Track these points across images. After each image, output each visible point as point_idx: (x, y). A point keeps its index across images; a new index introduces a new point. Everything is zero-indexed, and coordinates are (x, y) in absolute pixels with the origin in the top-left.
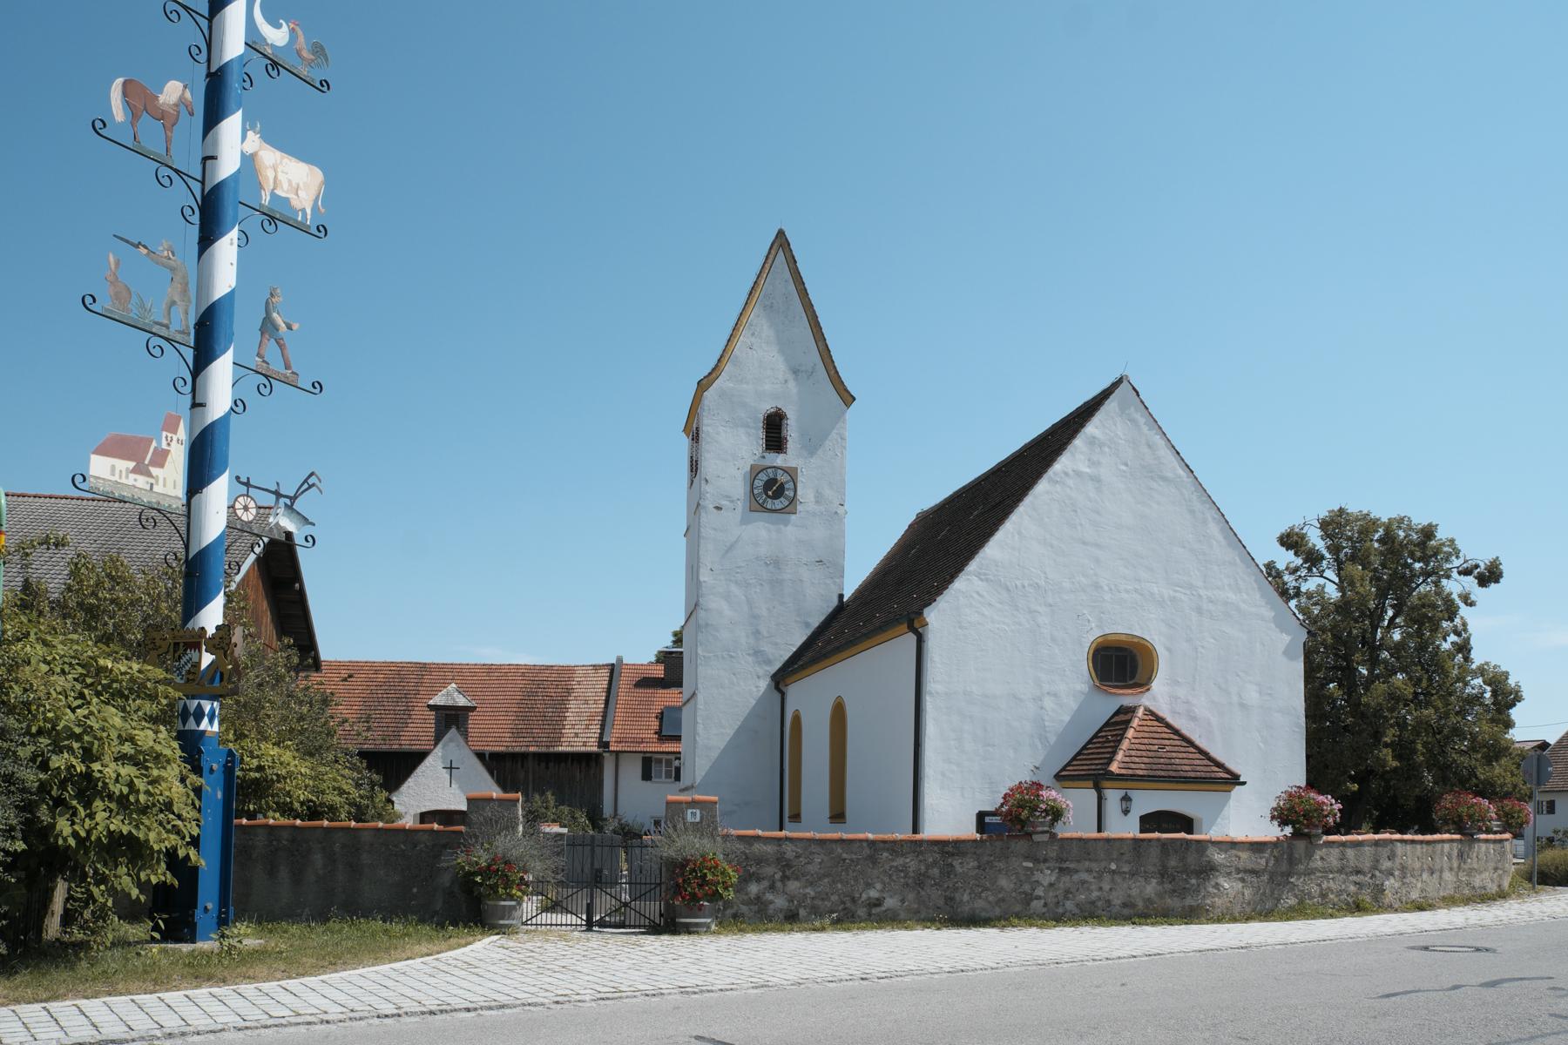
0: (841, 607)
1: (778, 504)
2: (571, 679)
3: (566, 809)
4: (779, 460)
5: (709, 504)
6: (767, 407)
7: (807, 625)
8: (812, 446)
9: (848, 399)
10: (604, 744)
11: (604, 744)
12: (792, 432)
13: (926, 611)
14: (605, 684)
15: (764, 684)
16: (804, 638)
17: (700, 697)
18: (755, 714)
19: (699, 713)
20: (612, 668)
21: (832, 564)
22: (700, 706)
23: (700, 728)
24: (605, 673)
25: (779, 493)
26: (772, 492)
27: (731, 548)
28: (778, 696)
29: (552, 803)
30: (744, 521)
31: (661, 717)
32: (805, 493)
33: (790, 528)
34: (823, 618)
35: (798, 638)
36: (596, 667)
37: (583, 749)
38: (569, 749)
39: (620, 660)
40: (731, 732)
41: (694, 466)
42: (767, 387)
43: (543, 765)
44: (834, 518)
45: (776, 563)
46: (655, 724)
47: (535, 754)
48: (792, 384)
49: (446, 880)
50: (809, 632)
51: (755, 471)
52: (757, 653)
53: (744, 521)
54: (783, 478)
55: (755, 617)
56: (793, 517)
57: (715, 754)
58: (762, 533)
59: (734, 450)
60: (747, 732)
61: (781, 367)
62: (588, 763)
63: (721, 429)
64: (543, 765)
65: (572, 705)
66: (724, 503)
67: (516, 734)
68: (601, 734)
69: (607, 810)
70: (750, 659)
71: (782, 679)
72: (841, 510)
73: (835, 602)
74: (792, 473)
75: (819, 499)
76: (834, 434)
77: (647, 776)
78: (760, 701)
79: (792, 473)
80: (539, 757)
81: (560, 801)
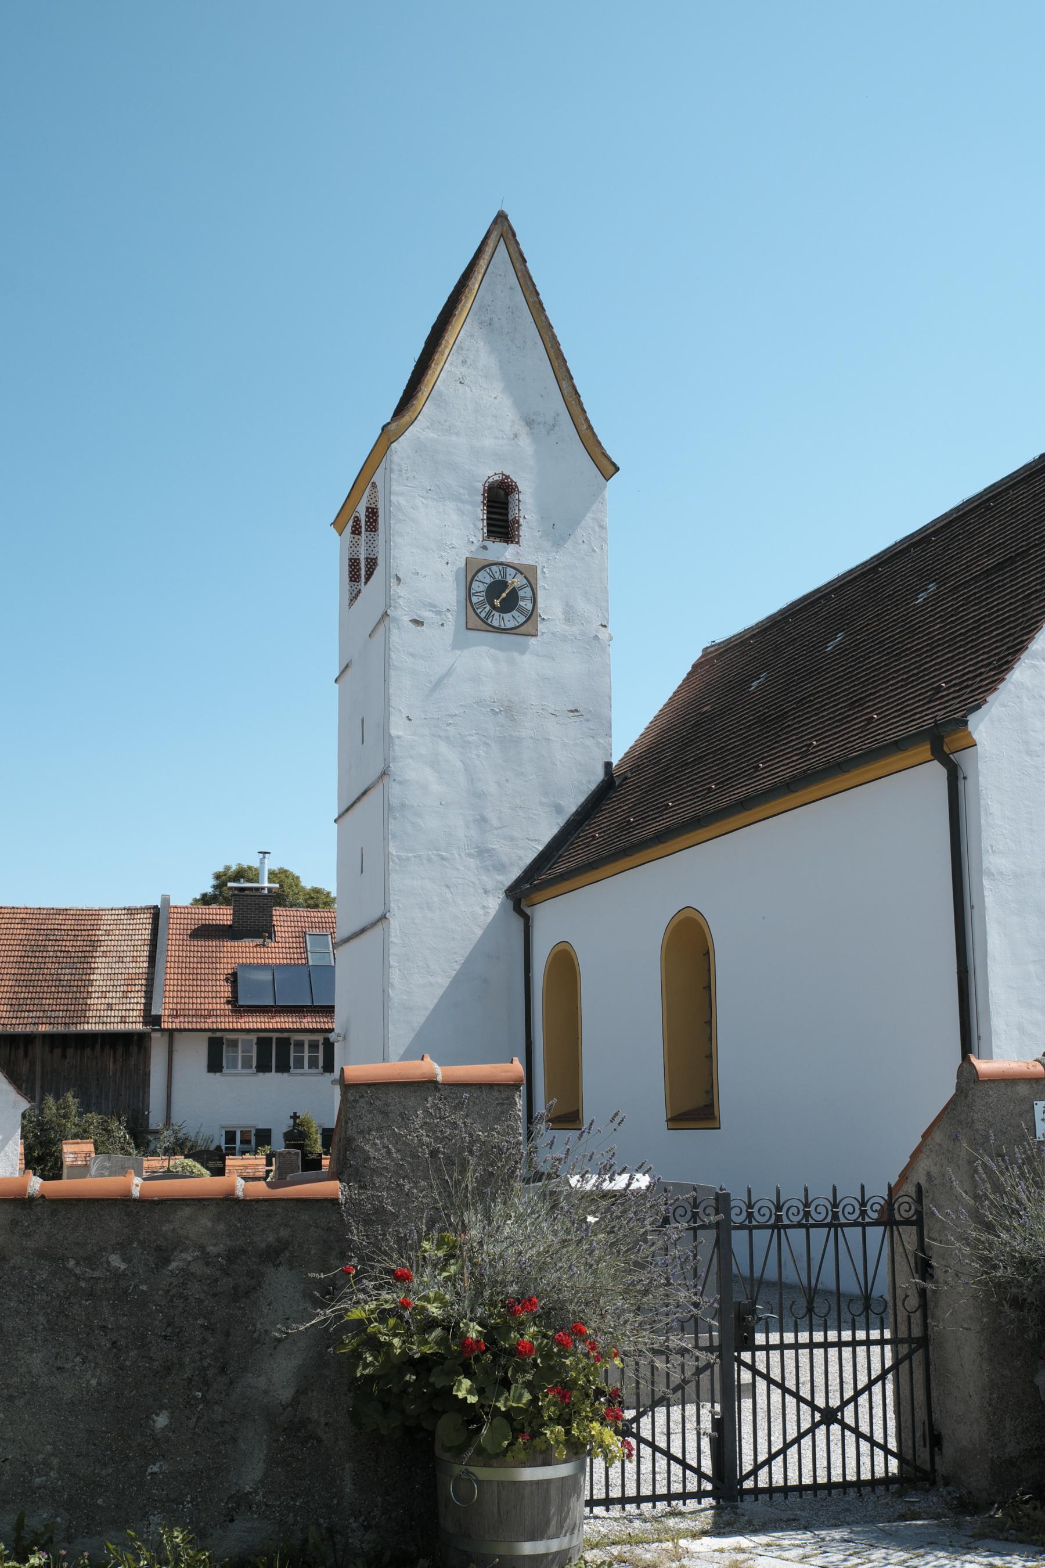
0: (610, 786)
1: (509, 620)
2: (95, 927)
3: (94, 1117)
4: (508, 553)
5: (402, 614)
6: (488, 472)
7: (559, 809)
8: (559, 533)
9: (608, 468)
10: (152, 1020)
11: (152, 1020)
12: (527, 510)
13: (972, 719)
14: (147, 934)
15: (495, 902)
16: (555, 830)
17: (395, 923)
18: (483, 952)
19: (393, 950)
20: (156, 913)
21: (590, 714)
22: (395, 937)
23: (395, 976)
24: (146, 919)
25: (510, 604)
26: (500, 602)
27: (438, 684)
28: (518, 923)
29: (74, 1109)
30: (458, 644)
31: (233, 979)
32: (550, 605)
33: (527, 658)
34: (581, 799)
35: (545, 831)
36: (131, 911)
37: (121, 1027)
38: (100, 1028)
39: (166, 900)
40: (444, 982)
41: (360, 571)
42: (488, 443)
43: (58, 1052)
44: (594, 645)
45: (508, 711)
46: (226, 990)
47: (45, 1036)
48: (525, 443)
49: (278, 1377)
50: (562, 821)
51: (472, 570)
52: (482, 852)
53: (458, 644)
54: (515, 581)
55: (480, 795)
56: (532, 641)
57: (419, 1019)
58: (485, 661)
59: (434, 540)
60: (468, 980)
61: (508, 415)
62: (128, 1047)
63: (419, 501)
64: (58, 1052)
65: (100, 963)
66: (426, 614)
67: (17, 1006)
68: (148, 1006)
69: (156, 1118)
70: (472, 862)
71: (525, 892)
72: (603, 634)
73: (599, 775)
74: (529, 574)
75: (570, 614)
76: (588, 520)
77: (215, 1065)
78: (490, 930)
79: (529, 574)
80: (51, 1039)
81: (86, 1107)
